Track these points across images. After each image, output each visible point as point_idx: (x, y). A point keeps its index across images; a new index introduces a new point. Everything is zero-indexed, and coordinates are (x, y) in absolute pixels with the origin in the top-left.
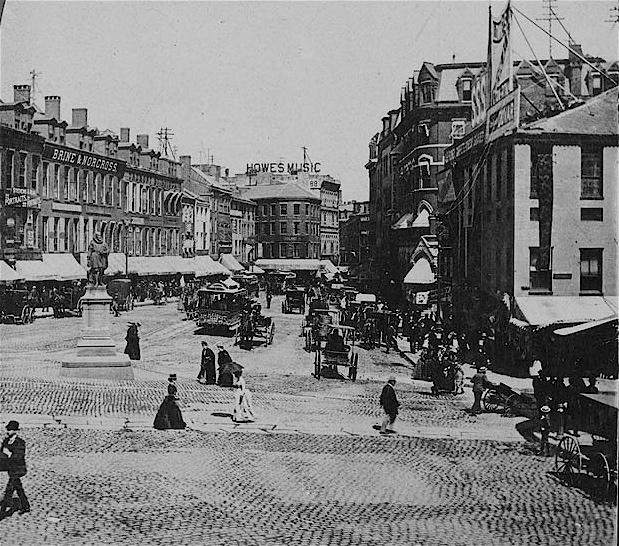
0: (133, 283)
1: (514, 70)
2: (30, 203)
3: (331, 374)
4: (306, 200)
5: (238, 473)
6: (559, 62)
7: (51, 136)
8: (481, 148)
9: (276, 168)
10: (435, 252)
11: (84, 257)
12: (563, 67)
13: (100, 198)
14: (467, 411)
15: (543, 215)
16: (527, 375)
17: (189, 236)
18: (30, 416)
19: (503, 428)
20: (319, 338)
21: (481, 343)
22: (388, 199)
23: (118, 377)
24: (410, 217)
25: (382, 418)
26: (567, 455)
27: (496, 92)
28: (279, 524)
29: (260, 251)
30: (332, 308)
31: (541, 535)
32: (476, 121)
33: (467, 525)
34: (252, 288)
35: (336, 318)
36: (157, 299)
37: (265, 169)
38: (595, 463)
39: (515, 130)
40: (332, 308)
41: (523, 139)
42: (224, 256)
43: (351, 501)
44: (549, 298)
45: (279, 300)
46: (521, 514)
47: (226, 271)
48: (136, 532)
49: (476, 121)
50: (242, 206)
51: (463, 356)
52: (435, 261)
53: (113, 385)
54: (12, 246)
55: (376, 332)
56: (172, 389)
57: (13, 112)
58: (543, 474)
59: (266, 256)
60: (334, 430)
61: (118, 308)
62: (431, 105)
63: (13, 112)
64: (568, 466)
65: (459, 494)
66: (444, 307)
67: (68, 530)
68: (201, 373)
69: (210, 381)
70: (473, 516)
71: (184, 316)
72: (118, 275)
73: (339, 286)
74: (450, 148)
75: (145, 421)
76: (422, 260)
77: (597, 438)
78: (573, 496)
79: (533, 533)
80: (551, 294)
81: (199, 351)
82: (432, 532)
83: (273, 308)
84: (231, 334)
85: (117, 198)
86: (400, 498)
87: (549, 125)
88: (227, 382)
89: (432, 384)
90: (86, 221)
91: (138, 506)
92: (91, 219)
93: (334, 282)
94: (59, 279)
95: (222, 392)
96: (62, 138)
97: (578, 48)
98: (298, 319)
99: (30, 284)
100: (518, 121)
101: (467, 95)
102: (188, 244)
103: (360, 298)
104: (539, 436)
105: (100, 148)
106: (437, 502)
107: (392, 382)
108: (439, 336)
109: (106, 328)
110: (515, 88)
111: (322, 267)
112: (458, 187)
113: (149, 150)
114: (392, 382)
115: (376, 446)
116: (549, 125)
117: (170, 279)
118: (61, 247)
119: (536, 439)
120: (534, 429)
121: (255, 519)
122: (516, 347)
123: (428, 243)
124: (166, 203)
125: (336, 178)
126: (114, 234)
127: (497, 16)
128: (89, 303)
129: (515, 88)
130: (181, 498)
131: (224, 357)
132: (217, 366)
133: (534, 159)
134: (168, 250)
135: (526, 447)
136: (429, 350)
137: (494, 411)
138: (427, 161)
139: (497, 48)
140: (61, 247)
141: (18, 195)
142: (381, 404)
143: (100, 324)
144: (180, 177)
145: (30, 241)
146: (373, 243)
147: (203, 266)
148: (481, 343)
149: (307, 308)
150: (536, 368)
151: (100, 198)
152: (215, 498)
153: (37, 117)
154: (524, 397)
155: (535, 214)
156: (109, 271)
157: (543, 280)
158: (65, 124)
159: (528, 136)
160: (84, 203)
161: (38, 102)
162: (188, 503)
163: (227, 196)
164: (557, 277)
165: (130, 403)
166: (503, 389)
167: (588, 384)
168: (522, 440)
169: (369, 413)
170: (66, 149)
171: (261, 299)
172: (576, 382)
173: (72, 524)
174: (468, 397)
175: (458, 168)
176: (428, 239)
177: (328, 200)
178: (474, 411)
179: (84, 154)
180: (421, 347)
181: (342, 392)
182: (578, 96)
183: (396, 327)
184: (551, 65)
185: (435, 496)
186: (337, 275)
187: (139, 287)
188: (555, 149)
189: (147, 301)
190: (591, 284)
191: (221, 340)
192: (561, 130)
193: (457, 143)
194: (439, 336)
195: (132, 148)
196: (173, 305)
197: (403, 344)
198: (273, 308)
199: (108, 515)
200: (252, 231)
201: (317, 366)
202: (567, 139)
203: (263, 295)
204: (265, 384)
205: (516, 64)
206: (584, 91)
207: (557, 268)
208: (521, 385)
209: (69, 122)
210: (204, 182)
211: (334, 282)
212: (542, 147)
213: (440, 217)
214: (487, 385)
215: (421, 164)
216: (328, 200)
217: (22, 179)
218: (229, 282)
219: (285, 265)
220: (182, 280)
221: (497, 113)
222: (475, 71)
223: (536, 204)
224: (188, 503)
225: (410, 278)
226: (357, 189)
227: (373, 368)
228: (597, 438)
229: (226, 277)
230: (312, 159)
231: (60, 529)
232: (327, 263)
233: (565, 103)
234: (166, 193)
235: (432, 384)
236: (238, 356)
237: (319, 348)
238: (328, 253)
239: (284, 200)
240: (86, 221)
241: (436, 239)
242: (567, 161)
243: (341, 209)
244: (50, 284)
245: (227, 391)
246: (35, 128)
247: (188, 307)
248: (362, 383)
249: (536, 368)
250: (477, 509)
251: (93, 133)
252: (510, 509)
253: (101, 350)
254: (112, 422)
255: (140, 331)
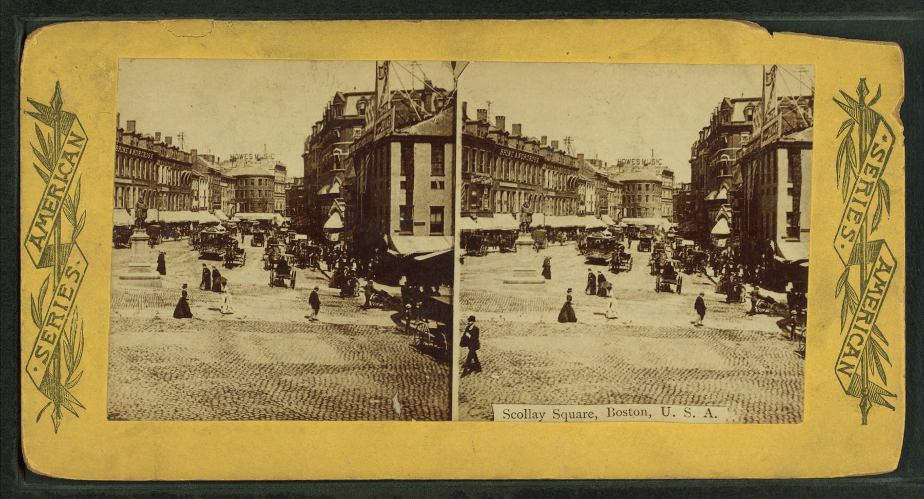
0: (548, 232)
1: (390, 97)
2: (486, 182)
3: (667, 289)
4: (265, 176)
5: (224, 345)
6: (419, 91)
7: (499, 141)
8: (371, 144)
9: (635, 162)
10: (343, 209)
11: (518, 216)
12: (807, 101)
13: (143, 175)
14: (747, 313)
15: (408, 186)
16: (396, 284)
17: (582, 204)
19: (383, 318)
20: (661, 267)
21: (757, 271)
22: (702, 180)
23: (152, 285)
24: (327, 187)
25: (696, 317)
26: (422, 334)
27: (768, 116)
28: (247, 376)
29: (625, 213)
30: (281, 243)
31: (790, 389)
32: (368, 127)
33: (361, 377)
34: (233, 231)
35: (283, 250)
36: (176, 237)
37: (629, 162)
38: (438, 340)
39: (778, 139)
40: (281, 243)
41: (783, 145)
43: (291, 363)
44: (411, 238)
45: (249, 238)
46: (778, 376)
48: (545, 385)
49: (368, 127)
50: (614, 185)
51: (746, 279)
52: (343, 214)
54: (475, 208)
55: (693, 265)
56: (185, 294)
57: (476, 126)
58: (407, 346)
61: (153, 243)
62: (340, 118)
63: (476, 126)
64: (422, 341)
65: (356, 358)
66: (735, 249)
67: (122, 379)
68: (202, 283)
69: (208, 288)
71: (192, 248)
72: (153, 223)
73: (672, 235)
74: (351, 145)
75: (168, 313)
76: (336, 214)
77: (440, 324)
78: (426, 359)
79: (785, 388)
81: (200, 270)
82: (339, 381)
83: (245, 243)
85: (538, 180)
86: (332, 362)
87: (413, 130)
89: (340, 291)
90: (520, 194)
91: (163, 365)
92: (523, 192)
93: (282, 227)
94: (504, 229)
96: (506, 142)
97: (430, 83)
98: (260, 251)
99: (486, 232)
100: (393, 128)
101: (363, 112)
102: (582, 208)
103: (298, 237)
104: (405, 322)
105: (143, 145)
106: (343, 363)
107: (317, 289)
108: (731, 266)
110: (392, 107)
111: (275, 218)
112: (745, 177)
113: (172, 146)
114: (317, 289)
116: (413, 130)
117: (184, 225)
118: (505, 209)
119: (788, 331)
122: (394, 267)
123: (339, 203)
125: (671, 169)
126: (536, 202)
127: (768, 70)
129: (392, 107)
130: (573, 365)
132: (597, 283)
133: (403, 151)
134: (570, 212)
135: (396, 329)
136: (339, 269)
137: (764, 313)
138: (726, 158)
139: (768, 89)
140: (505, 209)
141: (479, 177)
142: (696, 307)
143: (526, 257)
144: (190, 162)
145: (486, 206)
146: (306, 206)
147: (591, 222)
148: (757, 271)
149: (266, 243)
150: (403, 281)
151: (143, 175)
152: (210, 360)
153: (491, 129)
154: (781, 306)
155: (404, 185)
156: (148, 220)
157: (407, 227)
158: (507, 133)
160: (518, 182)
161: (492, 121)
162: (577, 368)
163: (606, 179)
164: (803, 231)
165: (161, 302)
166: (769, 300)
167: (434, 290)
168: (394, 325)
169: (302, 308)
170: (507, 148)
171: (238, 237)
172: (428, 290)
175: (744, 162)
176: (339, 201)
177: (279, 176)
178: (366, 307)
181: (287, 295)
182: (430, 111)
183: (319, 255)
184: (414, 94)
185: (342, 359)
186: (284, 223)
187: (552, 234)
188: (416, 145)
189: (170, 239)
190: (437, 229)
191: (214, 263)
192: (419, 134)
193: (357, 141)
194: (345, 261)
196: (185, 241)
198: (245, 243)
199: (146, 371)
200: (233, 196)
202: (422, 139)
204: (627, 295)
205: (779, 99)
206: (433, 109)
207: (416, 218)
208: (394, 291)
209: (510, 132)
210: (204, 166)
211: (282, 227)
212: (408, 143)
213: (346, 187)
214: (759, 297)
216: (279, 176)
217: (481, 167)
218: (220, 227)
219: (253, 217)
220: (191, 226)
221: (767, 129)
222: (368, 97)
223: (404, 179)
224: (577, 368)
225: (716, 230)
226: (296, 170)
227: (306, 280)
228: (440, 324)
229: (603, 229)
230: (269, 153)
231: (499, 382)
232: (278, 215)
233: (422, 116)
234: (569, 177)
235: (340, 291)
236: (224, 273)
238: (279, 209)
239: (640, 181)
241: (730, 206)
242: (422, 151)
243: (287, 182)
244: (498, 232)
245: (217, 295)
246: (489, 136)
247: (195, 243)
248: (298, 289)
249: (403, 281)
250: (752, 373)
251: (139, 136)
252: (771, 373)
253: (142, 269)
254: (148, 313)
255: (166, 257)
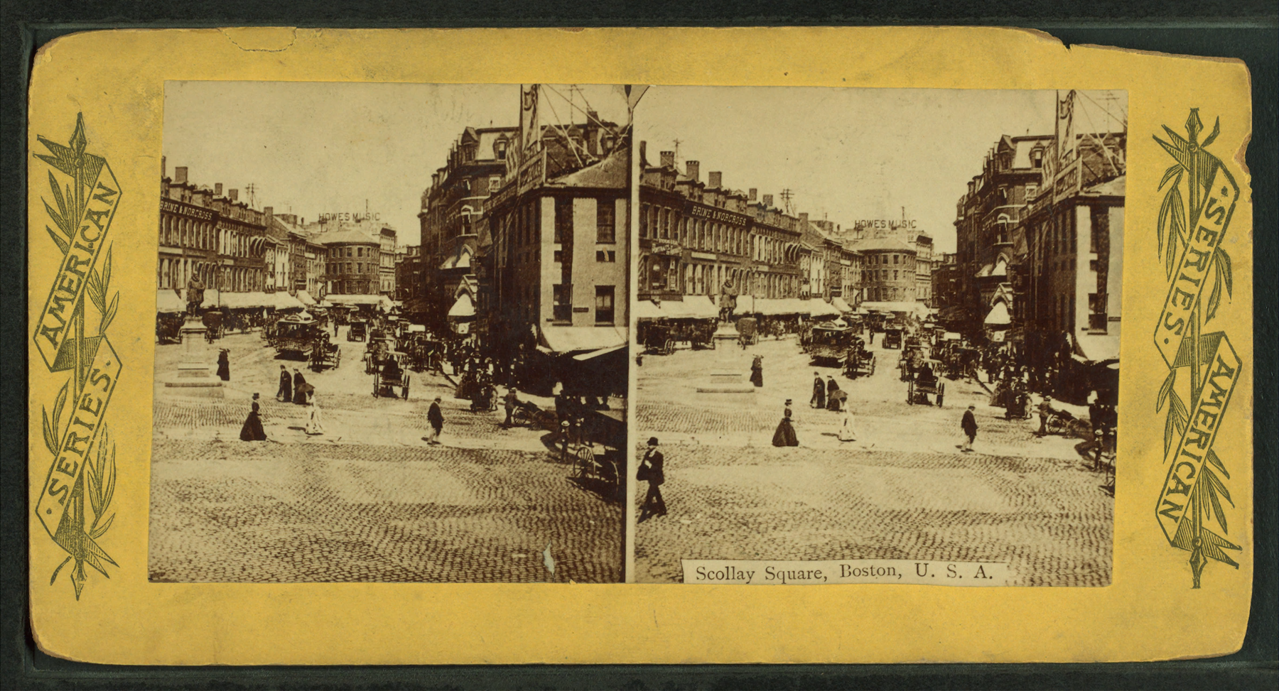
0: (758, 322)
1: (540, 134)
2: (673, 252)
3: (923, 400)
6: (579, 126)
8: (513, 199)
9: (879, 224)
10: (474, 289)
11: (717, 298)
12: (1118, 139)
13: (198, 243)
14: (1035, 433)
15: (565, 257)
16: (548, 393)
17: (806, 282)
18: (668, 433)
19: (530, 441)
21: (1047, 375)
22: (972, 250)
23: (210, 395)
24: (454, 258)
25: (963, 439)
26: (584, 463)
27: (1063, 161)
28: (343, 521)
29: (865, 295)
30: (389, 337)
31: (1093, 539)
32: (509, 177)
33: (500, 522)
34: (323, 320)
35: (392, 346)
36: (243, 328)
37: (870, 224)
38: (606, 471)
40: (389, 337)
41: (1085, 201)
42: (299, 292)
44: (569, 329)
45: (344, 330)
46: (1077, 521)
47: (301, 305)
48: (754, 533)
49: (509, 177)
50: (850, 256)
51: (1033, 387)
52: (475, 297)
53: (208, 403)
54: (658, 288)
55: (960, 367)
56: (256, 406)
57: (659, 175)
59: (334, 292)
60: (923, 449)
61: (212, 336)
63: (659, 175)
64: (584, 472)
66: (480, 335)
67: (169, 525)
68: (280, 392)
69: (287, 399)
70: (1036, 523)
71: (266, 343)
72: (212, 308)
74: (486, 201)
75: (232, 433)
77: (609, 448)
78: (590, 497)
79: (1086, 537)
80: (571, 325)
81: (278, 373)
82: (470, 528)
83: (339, 336)
84: (304, 359)
86: (460, 502)
87: (571, 180)
88: (301, 400)
89: (470, 402)
90: (720, 268)
91: (226, 505)
92: (724, 266)
93: (390, 314)
94: (697, 317)
95: (296, 409)
96: (700, 197)
97: (595, 115)
98: (360, 347)
99: (672, 321)
100: (544, 177)
101: (502, 155)
102: (805, 288)
103: (413, 328)
104: (560, 446)
106: (474, 502)
107: (438, 400)
109: (201, 354)
111: (381, 302)
112: (1031, 245)
113: (238, 202)
114: (438, 400)
115: (426, 456)
116: (571, 180)
117: (255, 312)
118: (698, 289)
119: (1091, 458)
120: (1089, 449)
121: (323, 518)
122: (545, 370)
123: (469, 282)
124: (251, 247)
126: (741, 279)
127: (1063, 97)
128: (188, 332)
130: (793, 506)
131: (833, 385)
132: (827, 392)
133: (558, 209)
134: (789, 293)
135: (549, 455)
136: (469, 372)
137: (1057, 433)
138: (1005, 219)
139: (1063, 124)
140: (698, 289)
141: (663, 245)
143: (728, 356)
144: (263, 224)
145: (673, 285)
146: (424, 285)
147: (817, 307)
148: (1047, 375)
150: (558, 389)
151: (198, 243)
152: (290, 499)
153: (679, 178)
154: (1082, 423)
155: (559, 256)
156: (205, 305)
157: (564, 314)
158: (702, 185)
159: (1086, 198)
160: (717, 252)
161: (681, 167)
162: (799, 509)
163: (303, 242)
164: (1112, 319)
165: (223, 418)
166: (1065, 415)
167: (601, 402)
168: (546, 450)
171: (329, 328)
172: (592, 401)
173: (172, 519)
174: (501, 413)
175: (1030, 225)
176: (469, 278)
177: (386, 244)
178: (506, 425)
179: (184, 205)
180: (997, 378)
181: (397, 408)
182: (595, 154)
183: (442, 353)
184: (573, 130)
185: (473, 497)
186: (393, 309)
187: (765, 324)
188: (575, 201)
189: (236, 330)
190: (605, 317)
191: (296, 364)
192: (580, 185)
193: (494, 195)
195: (759, 206)
196: (257, 333)
197: (448, 368)
198: (339, 336)
199: (202, 513)
200: (323, 271)
201: (376, 387)
202: (585, 193)
203: (867, 332)
204: (867, 408)
205: (1079, 137)
206: (600, 151)
207: (576, 302)
208: (545, 403)
209: (706, 182)
210: (282, 229)
211: (390, 314)
212: (565, 198)
213: (479, 259)
214: (1051, 411)
215: (464, 214)
216: (386, 244)
218: (304, 314)
219: (350, 300)
220: (265, 313)
221: (526, 171)
222: (509, 135)
223: (559, 247)
224: (799, 509)
225: (992, 318)
226: (410, 235)
227: (423, 387)
228: (609, 448)
229: (835, 317)
230: (372, 211)
231: (691, 529)
232: (385, 298)
233: (584, 161)
234: (787, 245)
235: (470, 402)
236: (310, 378)
237: (378, 371)
238: (386, 289)
239: (349, 244)
240: (720, 268)
242: (584, 210)
243: (397, 252)
245: (300, 408)
246: (677, 188)
247: (804, 343)
248: (412, 401)
249: (558, 389)
251: (192, 188)
253: (197, 373)
254: (205, 434)
255: (230, 356)
